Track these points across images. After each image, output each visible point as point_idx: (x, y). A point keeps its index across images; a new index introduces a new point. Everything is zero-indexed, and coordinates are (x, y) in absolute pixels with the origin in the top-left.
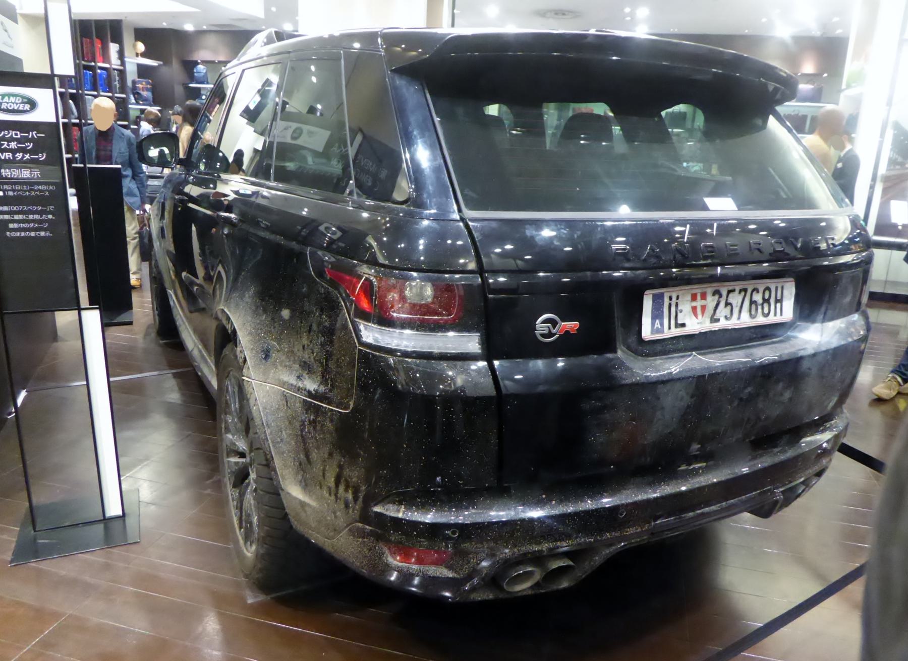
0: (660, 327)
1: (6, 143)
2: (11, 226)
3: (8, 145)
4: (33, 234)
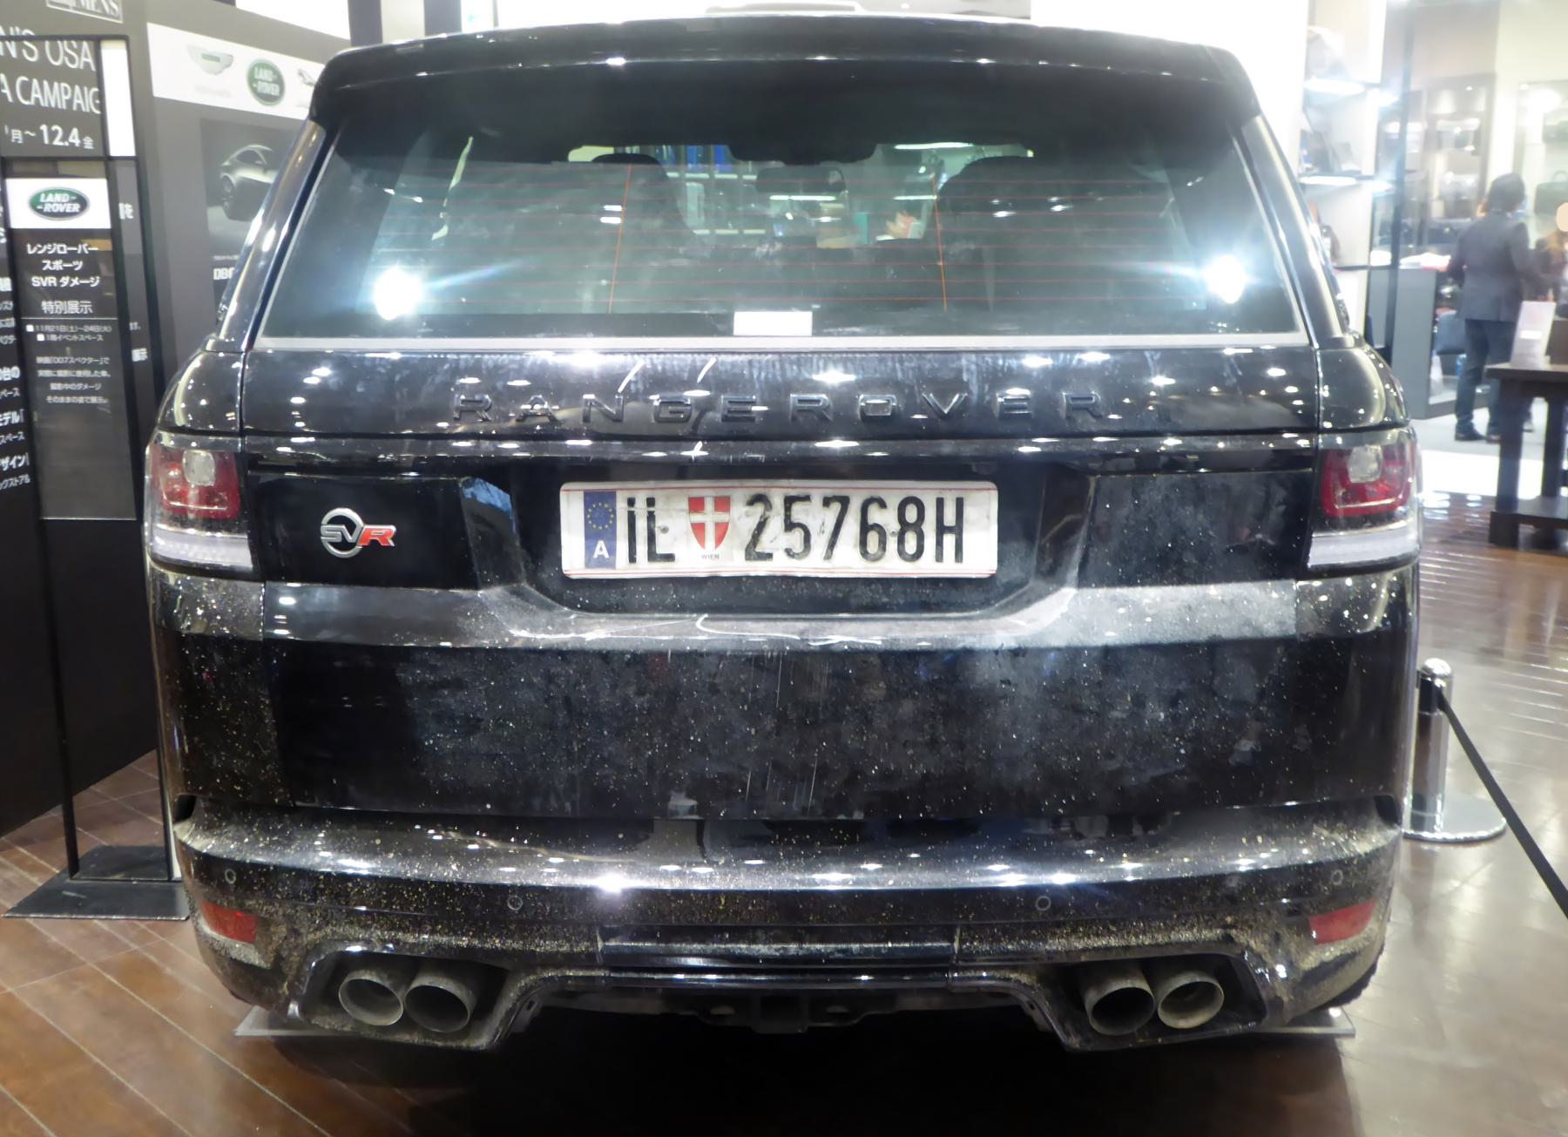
0: (607, 556)
1: (48, 262)
2: (54, 386)
3: (52, 265)
4: (81, 400)
